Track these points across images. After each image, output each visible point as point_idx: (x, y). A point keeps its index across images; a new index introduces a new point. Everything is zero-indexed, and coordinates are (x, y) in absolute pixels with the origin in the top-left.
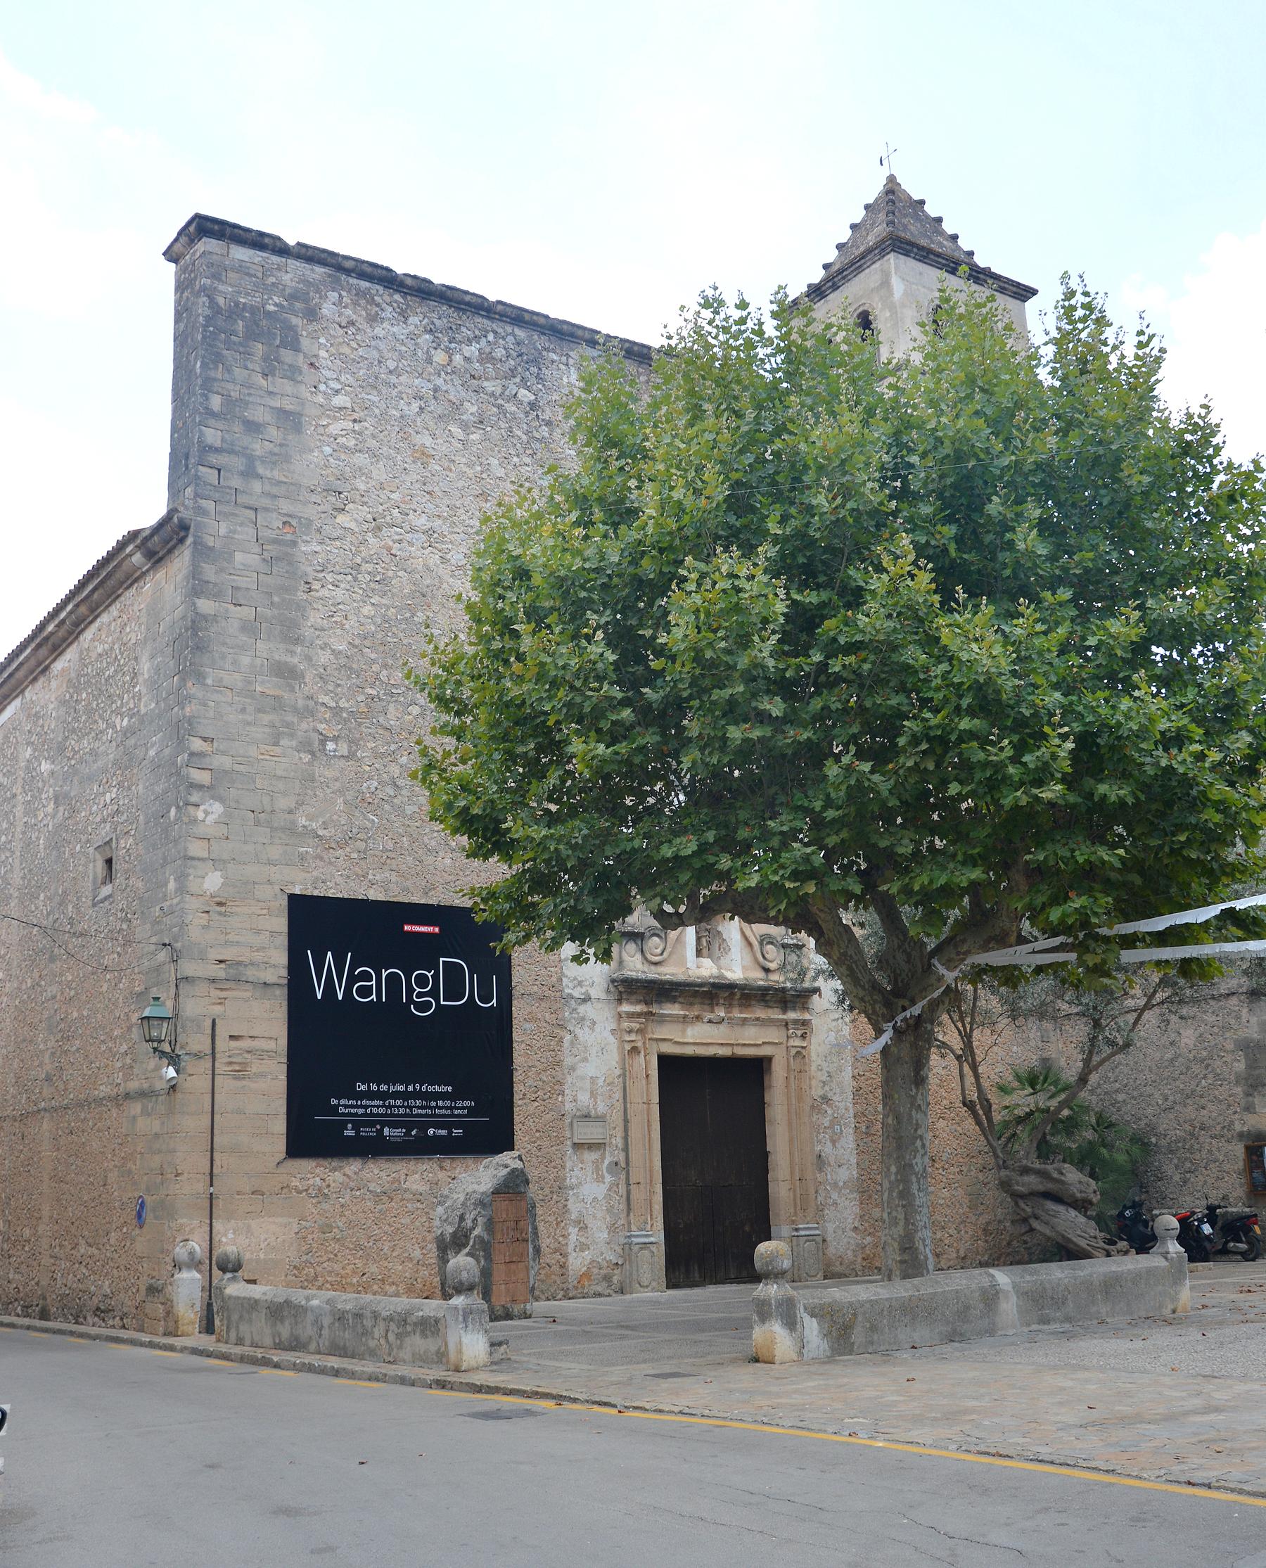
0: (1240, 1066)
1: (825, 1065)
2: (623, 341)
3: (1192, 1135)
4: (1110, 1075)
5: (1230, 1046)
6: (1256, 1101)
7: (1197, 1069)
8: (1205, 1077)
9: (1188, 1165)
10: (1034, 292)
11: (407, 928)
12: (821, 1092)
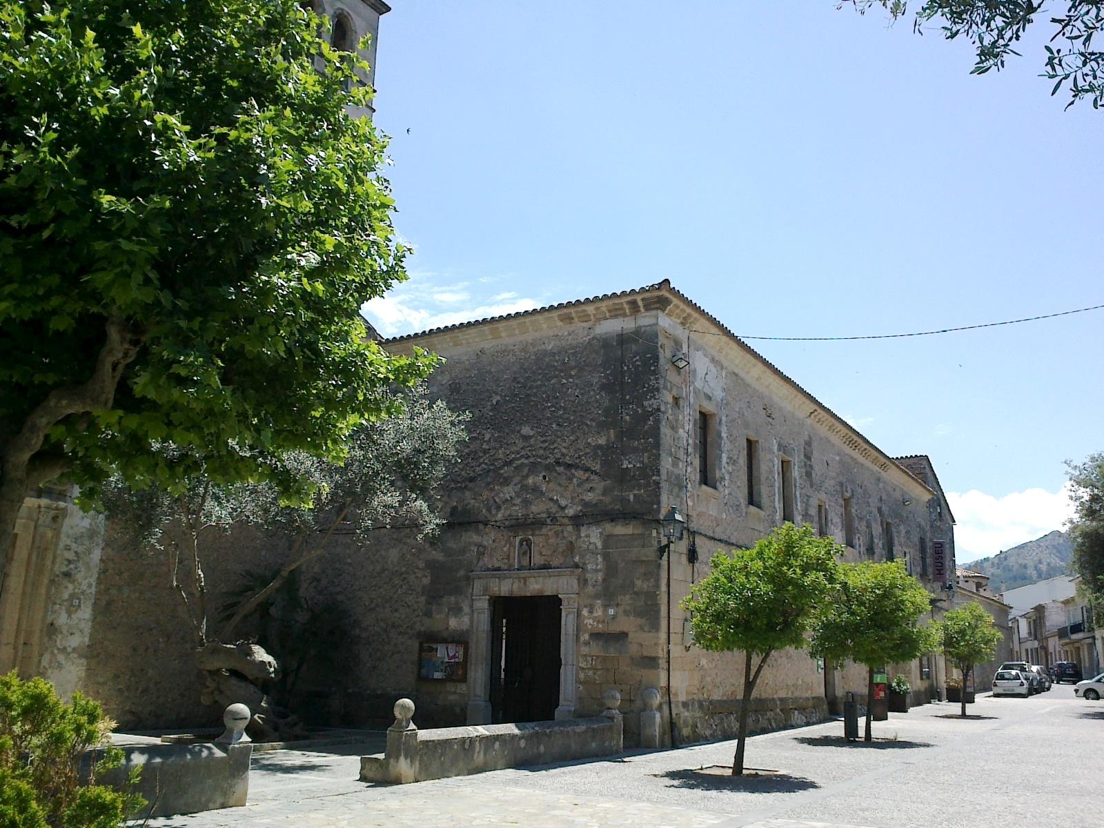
0: (426, 581)
1: (74, 546)
2: (626, 731)
3: (385, 630)
4: (335, 580)
5: (421, 565)
6: (434, 608)
7: (396, 581)
8: (401, 587)
9: (379, 654)
10: (389, 9)
11: (504, 621)
12: (64, 569)
